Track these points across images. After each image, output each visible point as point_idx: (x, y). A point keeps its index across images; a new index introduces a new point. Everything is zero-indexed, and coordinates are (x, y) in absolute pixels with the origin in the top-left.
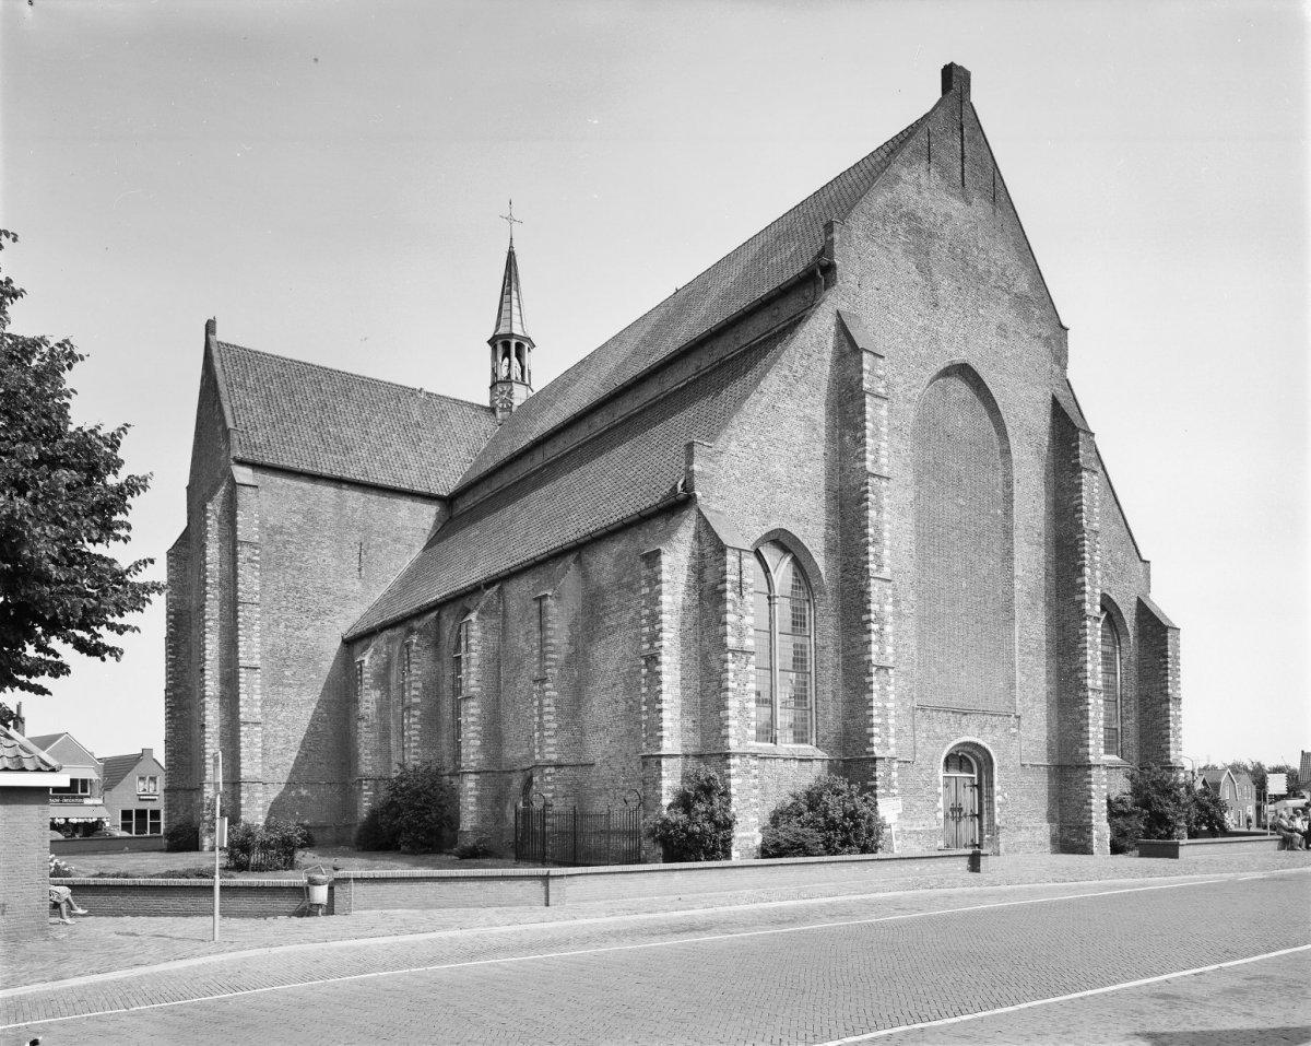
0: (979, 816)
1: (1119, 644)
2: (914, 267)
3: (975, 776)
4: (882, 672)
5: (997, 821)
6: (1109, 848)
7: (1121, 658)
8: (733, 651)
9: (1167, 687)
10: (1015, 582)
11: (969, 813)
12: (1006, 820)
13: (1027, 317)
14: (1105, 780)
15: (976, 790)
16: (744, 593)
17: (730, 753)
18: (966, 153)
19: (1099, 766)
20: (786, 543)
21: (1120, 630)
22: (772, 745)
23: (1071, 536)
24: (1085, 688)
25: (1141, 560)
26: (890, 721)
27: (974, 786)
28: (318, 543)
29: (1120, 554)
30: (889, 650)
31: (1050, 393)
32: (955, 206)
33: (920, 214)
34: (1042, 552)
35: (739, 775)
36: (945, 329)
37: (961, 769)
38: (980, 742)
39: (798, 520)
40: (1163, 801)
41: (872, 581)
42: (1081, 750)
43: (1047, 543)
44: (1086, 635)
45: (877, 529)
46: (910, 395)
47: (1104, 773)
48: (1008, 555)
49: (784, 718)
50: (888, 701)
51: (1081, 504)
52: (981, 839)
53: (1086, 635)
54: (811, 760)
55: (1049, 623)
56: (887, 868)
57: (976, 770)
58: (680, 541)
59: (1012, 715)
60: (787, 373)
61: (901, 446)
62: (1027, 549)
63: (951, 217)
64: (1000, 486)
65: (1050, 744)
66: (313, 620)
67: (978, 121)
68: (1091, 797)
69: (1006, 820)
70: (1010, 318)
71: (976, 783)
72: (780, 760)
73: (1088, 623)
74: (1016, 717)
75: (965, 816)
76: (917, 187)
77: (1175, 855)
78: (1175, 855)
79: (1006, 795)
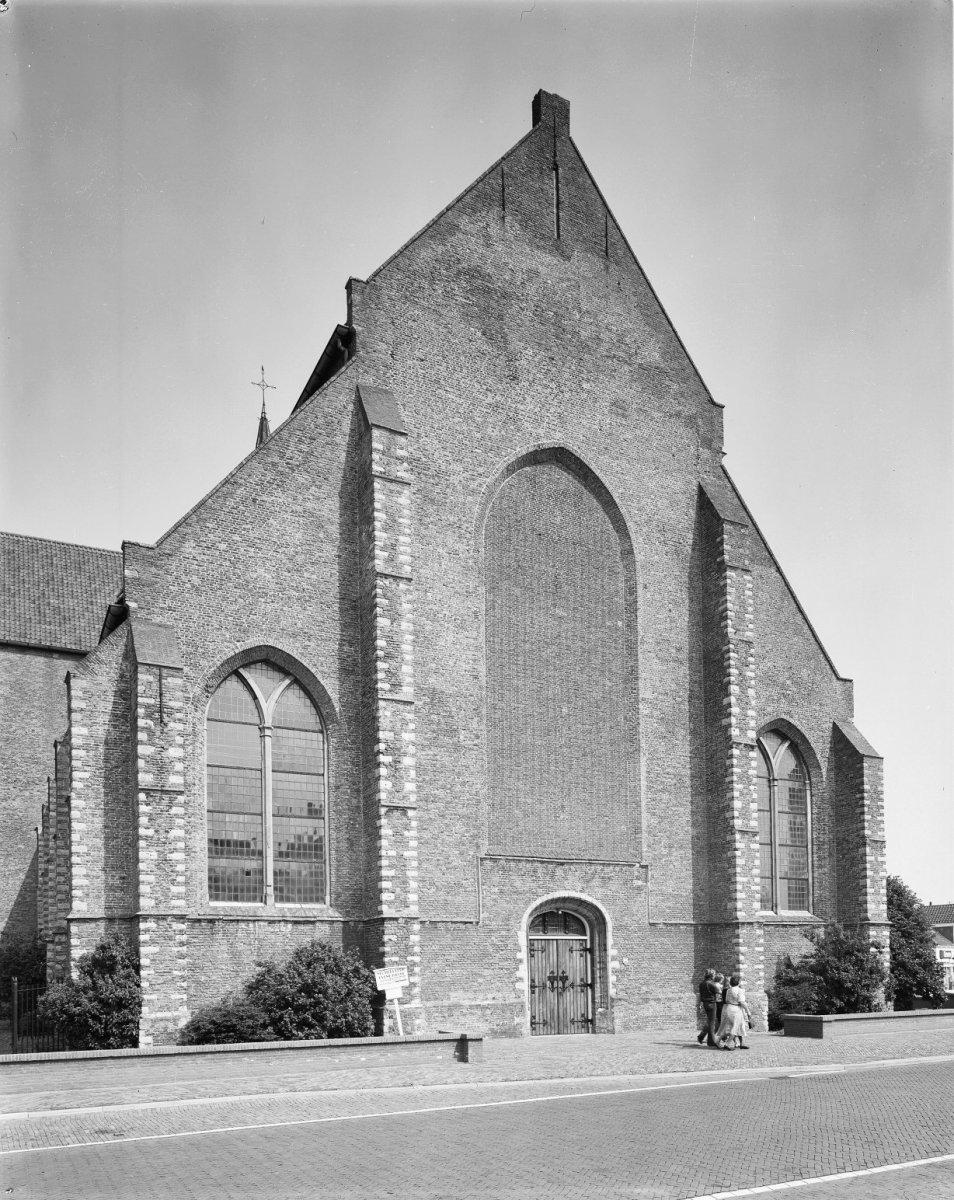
0: (592, 986)
1: (810, 779)
2: (479, 334)
3: (587, 938)
4: (397, 814)
5: (612, 992)
6: (766, 1023)
7: (812, 796)
8: (147, 791)
9: (863, 828)
10: (641, 706)
11: (578, 982)
12: (625, 990)
13: (659, 392)
14: (762, 941)
15: (589, 956)
16: (166, 719)
17: (138, 916)
18: (563, 198)
19: (751, 923)
20: (784, 730)
21: (810, 762)
22: (262, 904)
23: (717, 650)
24: (731, 830)
25: (838, 679)
26: (410, 874)
27: (586, 950)
28: (27, 713)
29: (804, 673)
30: (410, 787)
31: (695, 482)
32: (545, 262)
33: (490, 270)
34: (684, 670)
35: (153, 942)
36: (530, 406)
37: (566, 929)
38: (584, 897)
39: (294, 635)
40: (843, 965)
41: (381, 704)
42: (730, 905)
43: (691, 660)
44: (732, 766)
45: (390, 640)
46: (473, 485)
47: (759, 932)
48: (632, 676)
49: (782, 888)
50: (407, 848)
51: (726, 610)
52: (594, 1014)
53: (732, 766)
54: (313, 923)
55: (695, 754)
56: (391, 1054)
57: (588, 933)
58: (100, 662)
59: (631, 866)
60: (276, 459)
61: (461, 547)
62: (657, 665)
63: (537, 273)
64: (622, 592)
65: (697, 898)
66: (21, 791)
67: (581, 159)
68: (738, 962)
69: (625, 990)
70: (631, 393)
71: (588, 947)
72: (262, 923)
73: (736, 752)
74: (642, 867)
75: (572, 985)
76: (510, 253)
77: (818, 1035)
78: (818, 1035)
79: (625, 960)
